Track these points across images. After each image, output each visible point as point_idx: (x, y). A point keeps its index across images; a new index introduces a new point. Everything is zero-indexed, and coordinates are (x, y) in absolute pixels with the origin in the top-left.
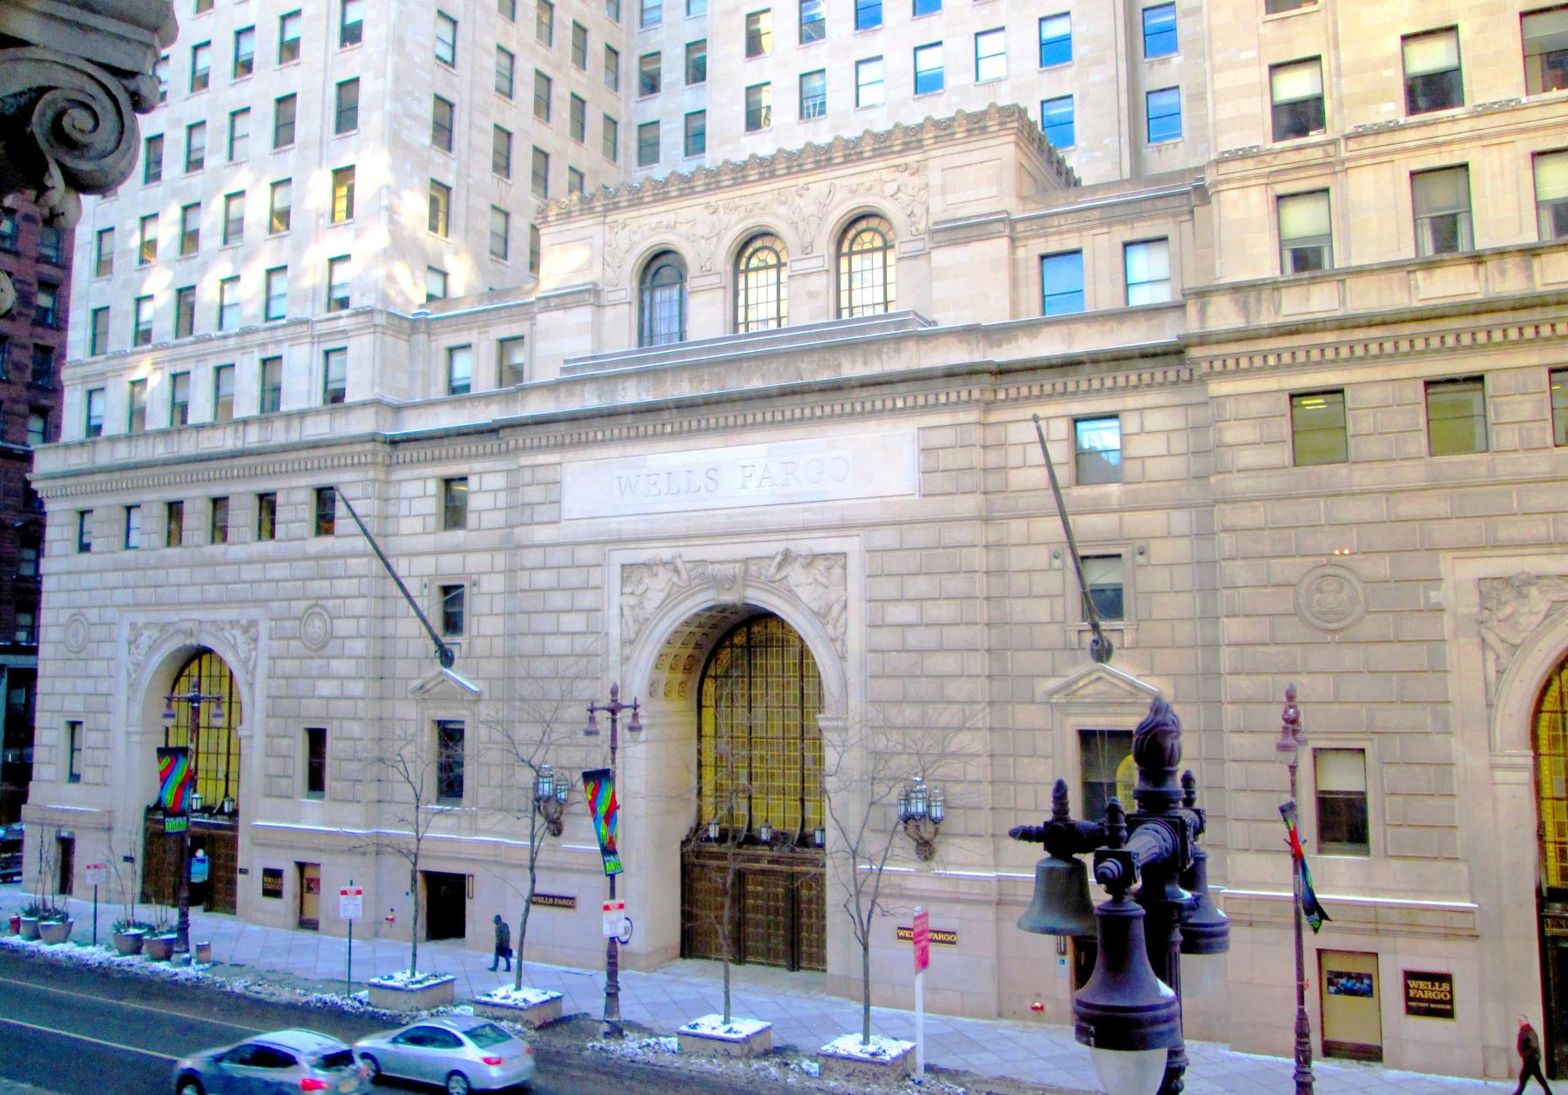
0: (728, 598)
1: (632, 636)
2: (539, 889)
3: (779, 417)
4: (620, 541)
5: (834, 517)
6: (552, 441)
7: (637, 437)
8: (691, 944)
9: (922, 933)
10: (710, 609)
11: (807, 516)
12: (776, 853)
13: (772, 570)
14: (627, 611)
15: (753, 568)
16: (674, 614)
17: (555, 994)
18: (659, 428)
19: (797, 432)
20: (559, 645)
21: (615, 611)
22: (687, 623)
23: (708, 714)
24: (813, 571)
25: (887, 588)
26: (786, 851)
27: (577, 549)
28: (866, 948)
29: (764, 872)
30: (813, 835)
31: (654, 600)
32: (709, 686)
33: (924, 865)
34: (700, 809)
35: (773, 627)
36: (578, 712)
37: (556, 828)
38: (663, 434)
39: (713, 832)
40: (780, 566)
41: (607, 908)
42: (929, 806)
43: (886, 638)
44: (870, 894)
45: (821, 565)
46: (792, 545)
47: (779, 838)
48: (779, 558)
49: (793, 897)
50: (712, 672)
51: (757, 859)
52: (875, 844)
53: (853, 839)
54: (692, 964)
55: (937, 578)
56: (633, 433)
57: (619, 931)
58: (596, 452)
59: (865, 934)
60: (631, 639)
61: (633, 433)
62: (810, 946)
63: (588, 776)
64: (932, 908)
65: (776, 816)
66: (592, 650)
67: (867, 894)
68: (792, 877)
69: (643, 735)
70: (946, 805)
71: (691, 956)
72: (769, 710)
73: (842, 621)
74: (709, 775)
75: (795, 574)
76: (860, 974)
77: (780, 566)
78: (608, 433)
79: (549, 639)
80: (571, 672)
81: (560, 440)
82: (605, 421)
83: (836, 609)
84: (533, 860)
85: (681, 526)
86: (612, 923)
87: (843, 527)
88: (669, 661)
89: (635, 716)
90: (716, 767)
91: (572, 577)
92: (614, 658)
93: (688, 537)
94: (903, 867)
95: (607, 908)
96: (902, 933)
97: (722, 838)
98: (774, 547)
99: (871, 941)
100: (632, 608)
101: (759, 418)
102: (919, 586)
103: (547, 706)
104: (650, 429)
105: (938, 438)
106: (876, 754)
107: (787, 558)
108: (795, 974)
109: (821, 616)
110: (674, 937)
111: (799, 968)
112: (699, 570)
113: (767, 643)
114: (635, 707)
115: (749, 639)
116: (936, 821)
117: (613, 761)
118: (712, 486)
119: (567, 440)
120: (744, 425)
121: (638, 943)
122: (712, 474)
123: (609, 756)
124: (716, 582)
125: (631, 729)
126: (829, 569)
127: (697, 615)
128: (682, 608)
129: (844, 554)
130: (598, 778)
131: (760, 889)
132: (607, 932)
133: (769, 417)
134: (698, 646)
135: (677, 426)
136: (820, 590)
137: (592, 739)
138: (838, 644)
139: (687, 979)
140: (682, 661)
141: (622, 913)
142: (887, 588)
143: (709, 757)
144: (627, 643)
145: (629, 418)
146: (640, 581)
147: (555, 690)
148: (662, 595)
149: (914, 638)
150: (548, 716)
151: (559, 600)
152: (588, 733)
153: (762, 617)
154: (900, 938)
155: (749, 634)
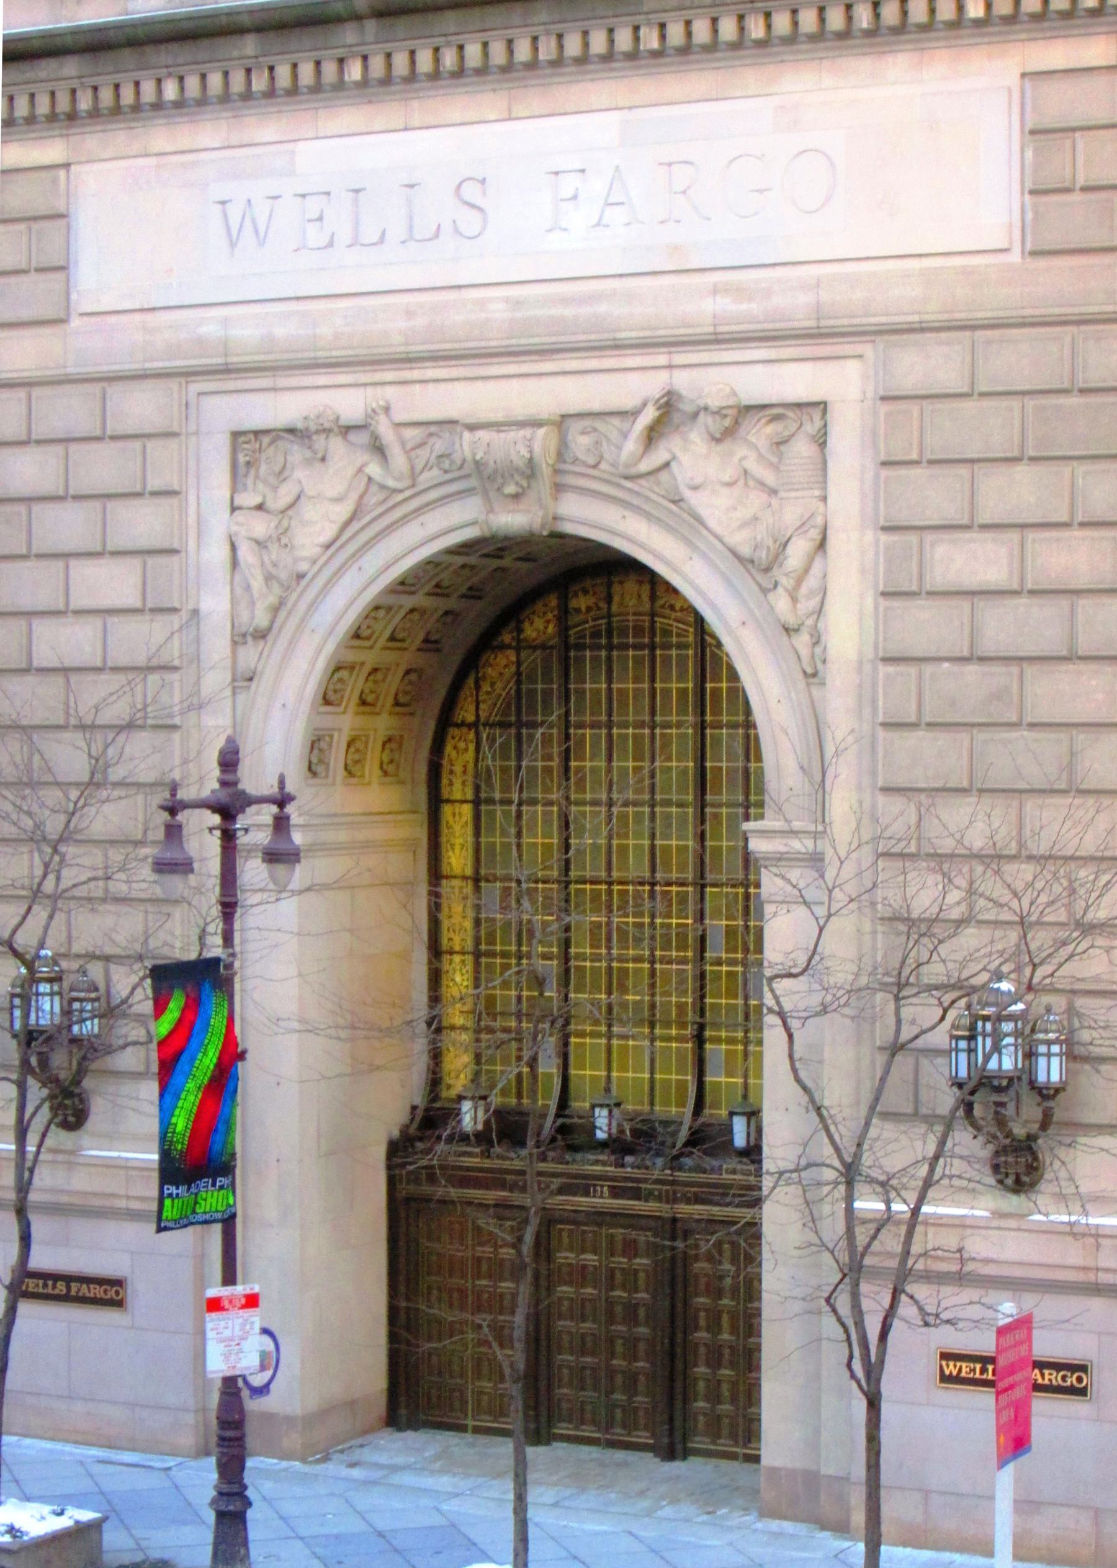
0: (512, 520)
1: (262, 619)
2: (39, 1260)
3: (650, 40)
4: (226, 370)
5: (794, 304)
6: (43, 106)
7: (271, 93)
8: (417, 1393)
9: (1012, 1370)
10: (464, 548)
11: (725, 305)
12: (630, 1166)
13: (631, 446)
14: (246, 553)
15: (580, 442)
16: (372, 561)
17: (87, 1515)
18: (330, 70)
19: (699, 80)
20: (71, 641)
21: (216, 553)
22: (403, 585)
23: (458, 821)
24: (741, 451)
25: (935, 496)
26: (658, 1169)
27: (115, 391)
28: (874, 1403)
29: (600, 1217)
30: (729, 1130)
31: (317, 525)
32: (460, 755)
33: (1013, 1202)
34: (436, 1056)
35: (629, 597)
36: (119, 815)
37: (71, 1110)
38: (340, 85)
39: (470, 1118)
40: (653, 435)
41: (215, 1305)
42: (1030, 1055)
43: (929, 626)
44: (874, 1272)
45: (760, 433)
46: (682, 381)
47: (639, 1138)
48: (649, 415)
49: (675, 1278)
50: (466, 712)
51: (583, 1185)
52: (899, 1149)
53: (846, 1135)
54: (423, 1444)
55: (1066, 470)
56: (259, 83)
57: (247, 1361)
58: (160, 136)
59: (873, 1372)
60: (254, 630)
61: (259, 83)
62: (715, 1397)
63: (166, 977)
64: (1045, 1307)
65: (632, 1076)
66: (164, 658)
67: (877, 1273)
68: (674, 1227)
69: (300, 875)
70: (1073, 1055)
71: (413, 1424)
72: (614, 804)
73: (812, 582)
74: (459, 977)
75: (692, 457)
76: (859, 1471)
77: (653, 435)
78: (193, 83)
79: (43, 629)
80: (117, 712)
81: (63, 104)
82: (183, 53)
83: (798, 551)
84: (23, 1187)
85: (392, 327)
86: (234, 1344)
87: (820, 336)
88: (356, 684)
89: (281, 824)
90: (477, 955)
91: (102, 468)
92: (215, 680)
93: (408, 360)
94: (967, 1211)
95: (215, 1305)
96: (951, 1368)
97: (508, 1128)
98: (634, 386)
99: (887, 1387)
100: (260, 544)
101: (598, 43)
102: (1018, 491)
103: (53, 796)
104: (306, 72)
105: (1064, 103)
106: (911, 926)
107: (669, 414)
108: (677, 1467)
109: (759, 567)
110: (371, 1375)
111: (686, 1454)
112: (438, 446)
113: (609, 635)
114: (282, 800)
115: (564, 629)
116: (1047, 1094)
117: (228, 939)
118: (470, 221)
119: (85, 103)
120: (558, 62)
121: (287, 1397)
122: (470, 192)
123: (216, 927)
124: (486, 478)
125: (272, 857)
126: (780, 443)
127: (431, 563)
128: (394, 544)
129: (822, 406)
130: (197, 982)
131: (590, 1258)
132: (217, 1364)
133: (624, 40)
134: (430, 644)
135: (377, 65)
136: (756, 500)
137: (176, 884)
138: (802, 641)
139: (407, 1479)
140: (393, 683)
141: (255, 1319)
142: (935, 496)
143: (458, 928)
144: (246, 636)
145: (250, 45)
146: (281, 475)
147: (69, 758)
148: (343, 511)
149: (1001, 627)
150: (54, 825)
151: (67, 526)
152: (163, 867)
153: (613, 567)
154: (945, 1379)
155: (564, 612)
